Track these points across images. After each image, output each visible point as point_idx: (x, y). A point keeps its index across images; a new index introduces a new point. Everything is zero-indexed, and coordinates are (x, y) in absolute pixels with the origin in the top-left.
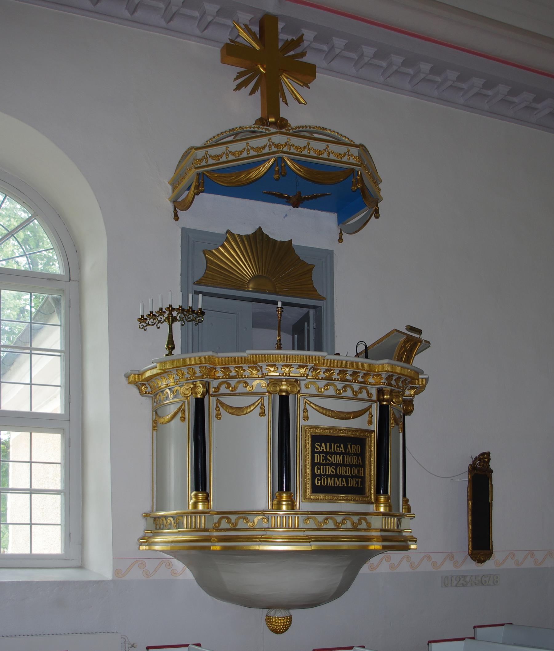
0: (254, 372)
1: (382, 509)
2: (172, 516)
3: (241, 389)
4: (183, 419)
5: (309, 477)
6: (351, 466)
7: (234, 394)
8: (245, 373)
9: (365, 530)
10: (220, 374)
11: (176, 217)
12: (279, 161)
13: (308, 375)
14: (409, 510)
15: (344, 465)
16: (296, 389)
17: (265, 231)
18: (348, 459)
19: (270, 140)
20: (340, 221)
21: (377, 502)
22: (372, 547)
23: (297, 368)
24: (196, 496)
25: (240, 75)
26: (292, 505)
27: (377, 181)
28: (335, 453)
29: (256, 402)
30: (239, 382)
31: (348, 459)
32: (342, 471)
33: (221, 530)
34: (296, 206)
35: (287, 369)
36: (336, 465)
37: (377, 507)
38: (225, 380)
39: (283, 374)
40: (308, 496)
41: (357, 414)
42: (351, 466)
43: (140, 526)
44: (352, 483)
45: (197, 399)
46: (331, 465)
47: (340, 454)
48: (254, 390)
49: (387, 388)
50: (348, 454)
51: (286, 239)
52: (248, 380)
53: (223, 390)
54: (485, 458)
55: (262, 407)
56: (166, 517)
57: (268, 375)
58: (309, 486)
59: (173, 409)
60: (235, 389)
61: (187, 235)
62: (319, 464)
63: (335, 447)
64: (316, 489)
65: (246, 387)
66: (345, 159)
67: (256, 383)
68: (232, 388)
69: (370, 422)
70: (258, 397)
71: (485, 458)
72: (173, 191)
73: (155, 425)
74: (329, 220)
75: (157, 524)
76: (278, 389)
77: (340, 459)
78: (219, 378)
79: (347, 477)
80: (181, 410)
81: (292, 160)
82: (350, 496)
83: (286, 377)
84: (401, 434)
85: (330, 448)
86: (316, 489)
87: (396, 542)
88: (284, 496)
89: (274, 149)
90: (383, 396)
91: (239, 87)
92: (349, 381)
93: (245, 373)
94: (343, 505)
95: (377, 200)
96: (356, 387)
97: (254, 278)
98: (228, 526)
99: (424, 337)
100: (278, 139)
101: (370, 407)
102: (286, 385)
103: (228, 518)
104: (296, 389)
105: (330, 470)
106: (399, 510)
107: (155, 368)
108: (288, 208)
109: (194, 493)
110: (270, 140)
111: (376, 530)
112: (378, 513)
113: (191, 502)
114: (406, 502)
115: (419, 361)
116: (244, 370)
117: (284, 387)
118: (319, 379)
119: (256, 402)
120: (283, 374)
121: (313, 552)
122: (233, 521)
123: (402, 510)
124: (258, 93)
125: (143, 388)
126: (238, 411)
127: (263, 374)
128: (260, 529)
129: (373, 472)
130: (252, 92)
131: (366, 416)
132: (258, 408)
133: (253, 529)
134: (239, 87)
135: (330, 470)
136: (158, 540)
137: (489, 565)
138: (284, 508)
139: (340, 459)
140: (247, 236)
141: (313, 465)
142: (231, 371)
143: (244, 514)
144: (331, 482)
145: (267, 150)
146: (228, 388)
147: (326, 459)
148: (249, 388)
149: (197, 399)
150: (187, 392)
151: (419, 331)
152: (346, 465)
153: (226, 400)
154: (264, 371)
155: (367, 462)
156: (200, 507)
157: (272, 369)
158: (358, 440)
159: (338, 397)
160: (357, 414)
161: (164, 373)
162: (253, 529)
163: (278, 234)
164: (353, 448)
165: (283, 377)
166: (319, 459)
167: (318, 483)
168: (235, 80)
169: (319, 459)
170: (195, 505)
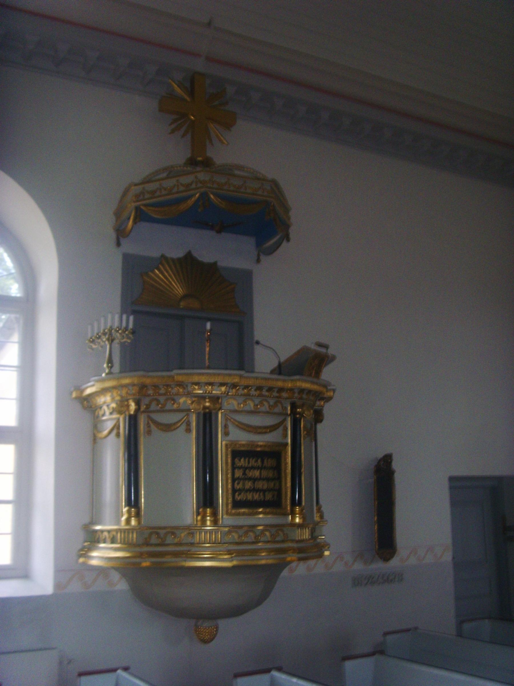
0: (181, 390)
1: (297, 520)
2: (109, 531)
3: (169, 406)
4: (118, 435)
5: (230, 491)
6: (268, 479)
7: (162, 411)
8: (173, 391)
9: (283, 541)
10: (151, 392)
11: (118, 244)
12: (204, 196)
13: (228, 392)
14: (322, 517)
15: (260, 479)
16: (218, 406)
17: (195, 254)
18: (265, 473)
19: (196, 177)
20: (259, 244)
21: (293, 513)
22: (289, 559)
23: (219, 386)
24: (129, 512)
25: (175, 121)
26: (215, 522)
27: (287, 209)
28: (253, 468)
29: (181, 420)
30: (167, 400)
31: (265, 473)
32: (260, 485)
33: (151, 545)
34: (219, 232)
35: (210, 387)
36: (254, 480)
37: (293, 518)
38: (155, 397)
39: (206, 393)
40: (230, 511)
41: (273, 428)
42: (268, 479)
43: (79, 540)
44: (269, 496)
45: (130, 416)
46: (250, 479)
47: (258, 468)
48: (182, 407)
49: (299, 403)
50: (265, 468)
51: (212, 261)
52: (175, 397)
53: (153, 407)
54: (387, 459)
55: (189, 424)
56: (102, 531)
57: (193, 393)
58: (230, 500)
59: (110, 425)
60: (164, 405)
61: (127, 259)
62: (238, 478)
63: (253, 463)
64: (237, 504)
65: (174, 404)
66: (260, 192)
67: (182, 400)
68: (162, 405)
69: (286, 436)
70: (184, 414)
71: (387, 459)
72: (117, 221)
73: (95, 439)
74: (248, 243)
75: (93, 539)
76: (202, 406)
77: (257, 473)
78: (149, 395)
79: (264, 491)
80: (117, 426)
81: (215, 195)
82: (268, 510)
83: (209, 395)
84: (314, 443)
85: (249, 463)
86: (237, 504)
87: (312, 550)
88: (208, 510)
89: (199, 185)
90: (296, 409)
91: (173, 131)
92: (266, 396)
93: (173, 391)
94: (262, 518)
95: (286, 226)
96: (272, 402)
97: (185, 297)
98: (159, 541)
99: (331, 351)
100: (202, 176)
101: (285, 420)
102: (209, 402)
103: (158, 534)
104: (218, 406)
105: (249, 485)
106: (313, 526)
107: (93, 385)
108: (212, 233)
109: (127, 509)
110: (196, 177)
111: (293, 541)
112: (293, 525)
113: (124, 518)
114: (319, 510)
115: (327, 373)
116: (172, 388)
117: (207, 404)
118: (238, 395)
119: (181, 420)
120: (206, 393)
121: (234, 567)
122: (162, 536)
123: (317, 518)
124: (189, 136)
125: (85, 402)
126: (168, 428)
127: (188, 392)
128: (187, 544)
129: (289, 484)
130: (183, 136)
131: (280, 430)
132: (184, 424)
133: (180, 544)
134: (173, 131)
135: (249, 485)
136: (95, 554)
137: (395, 562)
138: (208, 523)
139: (257, 473)
140: (179, 259)
141: (234, 480)
142: (160, 389)
143: (173, 531)
144: (250, 496)
145: (193, 186)
146: (158, 405)
147: (244, 474)
148: (175, 406)
149: (130, 416)
150: (123, 409)
151: (326, 347)
152: (263, 479)
153: (154, 416)
154: (190, 389)
155: (283, 475)
156: (133, 522)
157: (197, 387)
158: (274, 454)
159: (254, 412)
160: (273, 428)
161: (103, 391)
162: (180, 544)
163: (206, 256)
164: (269, 462)
165: (206, 395)
166: (238, 474)
167: (238, 498)
168: (170, 125)
169: (238, 474)
170: (128, 521)
